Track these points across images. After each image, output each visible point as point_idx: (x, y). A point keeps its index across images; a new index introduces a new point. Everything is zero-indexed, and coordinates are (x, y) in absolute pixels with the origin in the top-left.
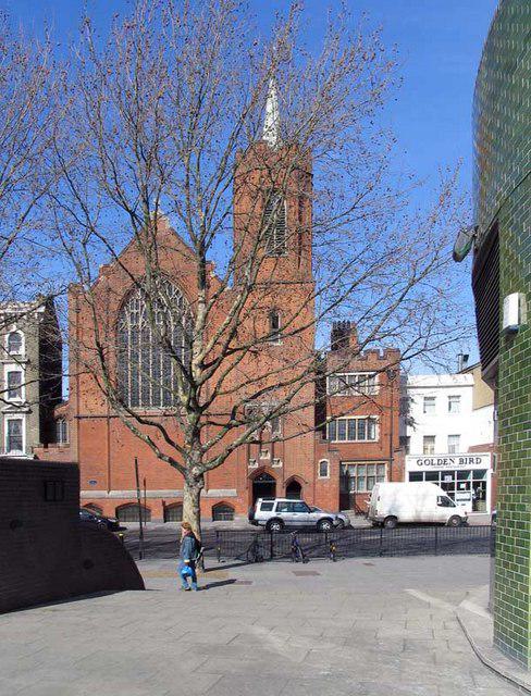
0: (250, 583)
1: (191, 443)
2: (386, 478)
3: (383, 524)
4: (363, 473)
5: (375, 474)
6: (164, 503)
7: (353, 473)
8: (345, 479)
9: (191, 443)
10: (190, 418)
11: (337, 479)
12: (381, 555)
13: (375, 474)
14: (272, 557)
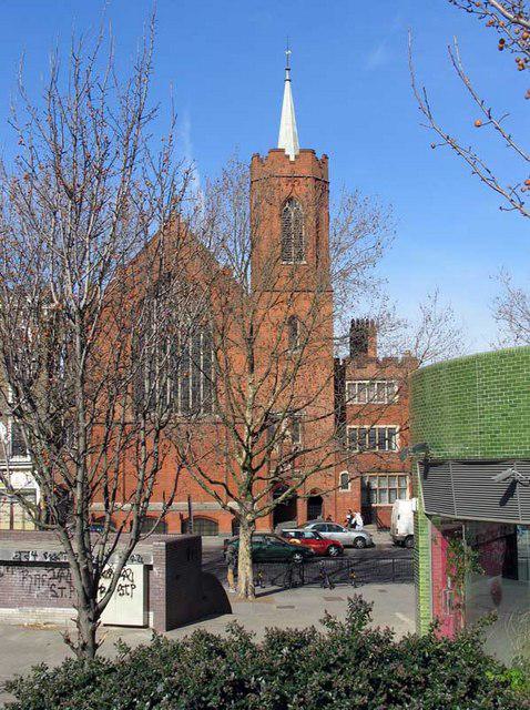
0: (293, 607)
1: (245, 495)
2: (408, 493)
3: (403, 542)
4: (384, 485)
5: (397, 486)
6: (181, 516)
7: (375, 485)
8: (367, 491)
9: (245, 495)
10: (244, 476)
11: (358, 493)
12: (394, 581)
13: (397, 486)
14: (302, 584)
